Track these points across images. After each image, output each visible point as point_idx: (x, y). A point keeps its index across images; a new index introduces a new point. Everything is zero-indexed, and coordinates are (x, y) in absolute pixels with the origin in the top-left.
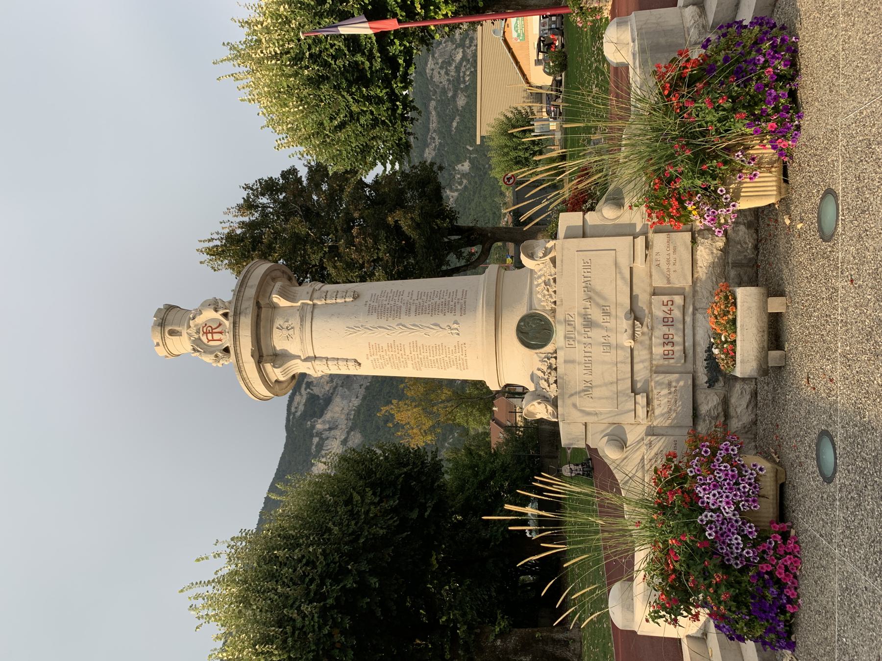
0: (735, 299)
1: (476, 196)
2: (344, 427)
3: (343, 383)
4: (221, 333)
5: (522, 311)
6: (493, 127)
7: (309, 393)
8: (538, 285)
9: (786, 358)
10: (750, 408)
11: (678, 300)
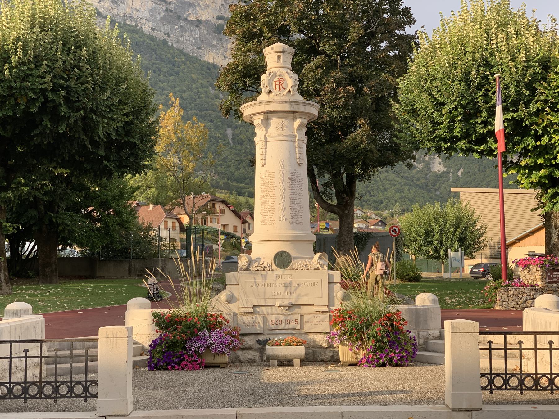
0: (299, 346)
1: (403, 180)
2: (115, 12)
3: (171, 11)
4: (280, 89)
5: (293, 253)
6: (466, 207)
8: (306, 262)
10: (247, 359)
11: (298, 327)
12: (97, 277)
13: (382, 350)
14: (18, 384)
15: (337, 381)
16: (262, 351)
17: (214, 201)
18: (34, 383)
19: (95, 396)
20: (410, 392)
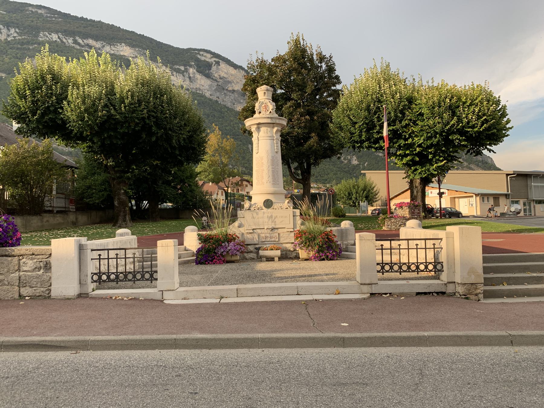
1: (337, 169)
2: (192, 86)
3: (220, 86)
5: (273, 200)
6: (369, 180)
7: (213, 63)
9: (264, 261)
11: (277, 240)
12: (180, 218)
13: (323, 251)
14: (122, 273)
15: (297, 269)
16: (258, 253)
17: (242, 180)
18: (130, 273)
19: (156, 279)
20: (337, 274)
